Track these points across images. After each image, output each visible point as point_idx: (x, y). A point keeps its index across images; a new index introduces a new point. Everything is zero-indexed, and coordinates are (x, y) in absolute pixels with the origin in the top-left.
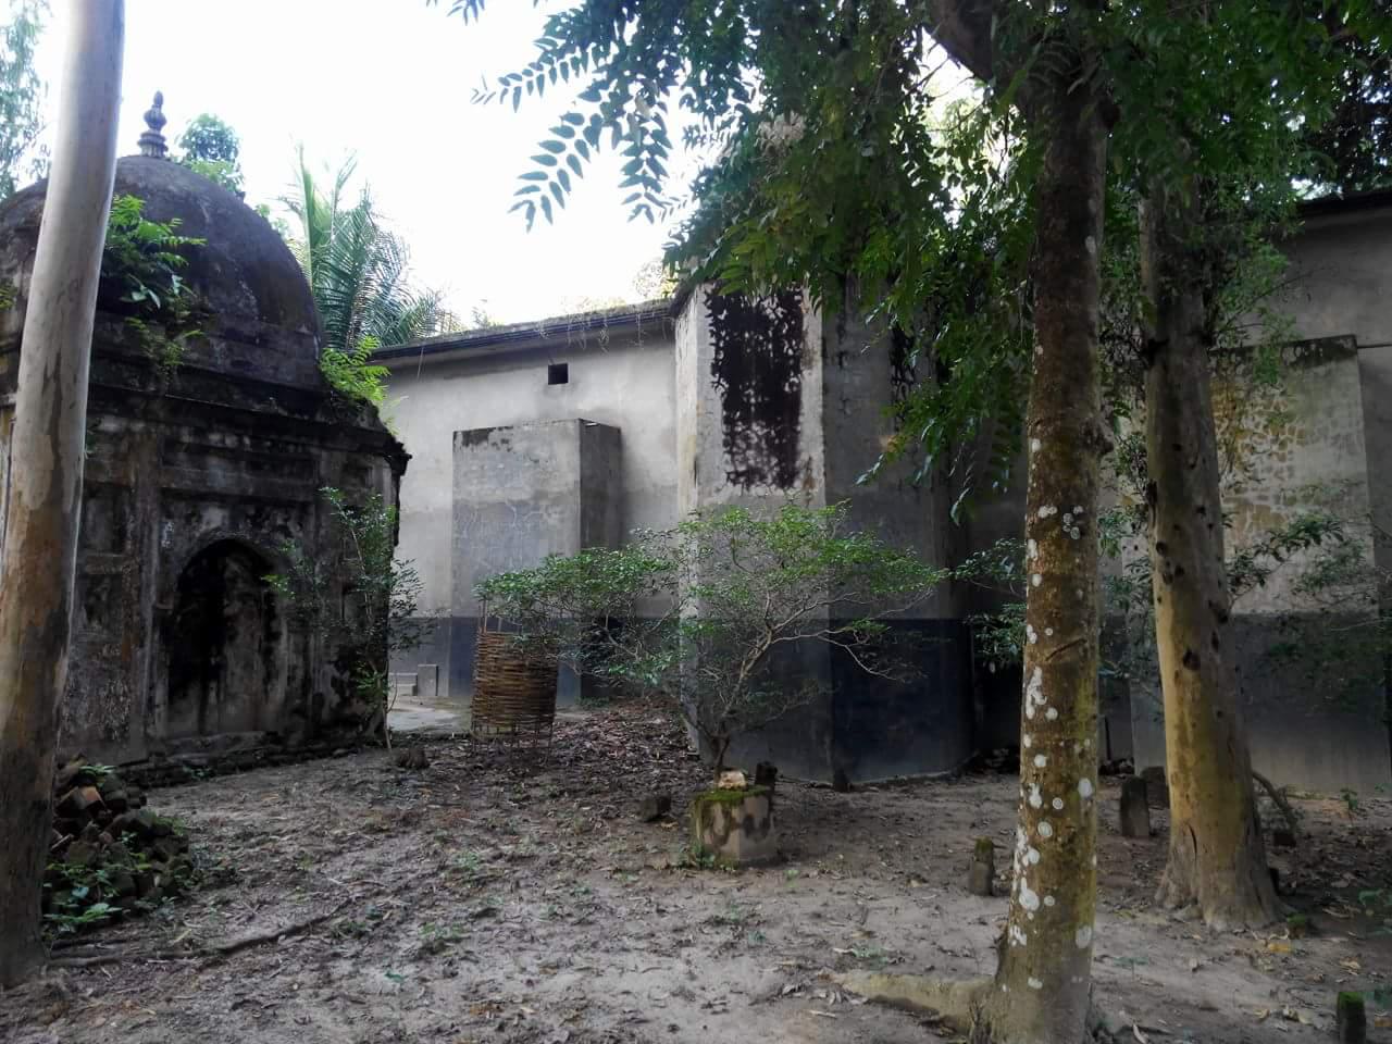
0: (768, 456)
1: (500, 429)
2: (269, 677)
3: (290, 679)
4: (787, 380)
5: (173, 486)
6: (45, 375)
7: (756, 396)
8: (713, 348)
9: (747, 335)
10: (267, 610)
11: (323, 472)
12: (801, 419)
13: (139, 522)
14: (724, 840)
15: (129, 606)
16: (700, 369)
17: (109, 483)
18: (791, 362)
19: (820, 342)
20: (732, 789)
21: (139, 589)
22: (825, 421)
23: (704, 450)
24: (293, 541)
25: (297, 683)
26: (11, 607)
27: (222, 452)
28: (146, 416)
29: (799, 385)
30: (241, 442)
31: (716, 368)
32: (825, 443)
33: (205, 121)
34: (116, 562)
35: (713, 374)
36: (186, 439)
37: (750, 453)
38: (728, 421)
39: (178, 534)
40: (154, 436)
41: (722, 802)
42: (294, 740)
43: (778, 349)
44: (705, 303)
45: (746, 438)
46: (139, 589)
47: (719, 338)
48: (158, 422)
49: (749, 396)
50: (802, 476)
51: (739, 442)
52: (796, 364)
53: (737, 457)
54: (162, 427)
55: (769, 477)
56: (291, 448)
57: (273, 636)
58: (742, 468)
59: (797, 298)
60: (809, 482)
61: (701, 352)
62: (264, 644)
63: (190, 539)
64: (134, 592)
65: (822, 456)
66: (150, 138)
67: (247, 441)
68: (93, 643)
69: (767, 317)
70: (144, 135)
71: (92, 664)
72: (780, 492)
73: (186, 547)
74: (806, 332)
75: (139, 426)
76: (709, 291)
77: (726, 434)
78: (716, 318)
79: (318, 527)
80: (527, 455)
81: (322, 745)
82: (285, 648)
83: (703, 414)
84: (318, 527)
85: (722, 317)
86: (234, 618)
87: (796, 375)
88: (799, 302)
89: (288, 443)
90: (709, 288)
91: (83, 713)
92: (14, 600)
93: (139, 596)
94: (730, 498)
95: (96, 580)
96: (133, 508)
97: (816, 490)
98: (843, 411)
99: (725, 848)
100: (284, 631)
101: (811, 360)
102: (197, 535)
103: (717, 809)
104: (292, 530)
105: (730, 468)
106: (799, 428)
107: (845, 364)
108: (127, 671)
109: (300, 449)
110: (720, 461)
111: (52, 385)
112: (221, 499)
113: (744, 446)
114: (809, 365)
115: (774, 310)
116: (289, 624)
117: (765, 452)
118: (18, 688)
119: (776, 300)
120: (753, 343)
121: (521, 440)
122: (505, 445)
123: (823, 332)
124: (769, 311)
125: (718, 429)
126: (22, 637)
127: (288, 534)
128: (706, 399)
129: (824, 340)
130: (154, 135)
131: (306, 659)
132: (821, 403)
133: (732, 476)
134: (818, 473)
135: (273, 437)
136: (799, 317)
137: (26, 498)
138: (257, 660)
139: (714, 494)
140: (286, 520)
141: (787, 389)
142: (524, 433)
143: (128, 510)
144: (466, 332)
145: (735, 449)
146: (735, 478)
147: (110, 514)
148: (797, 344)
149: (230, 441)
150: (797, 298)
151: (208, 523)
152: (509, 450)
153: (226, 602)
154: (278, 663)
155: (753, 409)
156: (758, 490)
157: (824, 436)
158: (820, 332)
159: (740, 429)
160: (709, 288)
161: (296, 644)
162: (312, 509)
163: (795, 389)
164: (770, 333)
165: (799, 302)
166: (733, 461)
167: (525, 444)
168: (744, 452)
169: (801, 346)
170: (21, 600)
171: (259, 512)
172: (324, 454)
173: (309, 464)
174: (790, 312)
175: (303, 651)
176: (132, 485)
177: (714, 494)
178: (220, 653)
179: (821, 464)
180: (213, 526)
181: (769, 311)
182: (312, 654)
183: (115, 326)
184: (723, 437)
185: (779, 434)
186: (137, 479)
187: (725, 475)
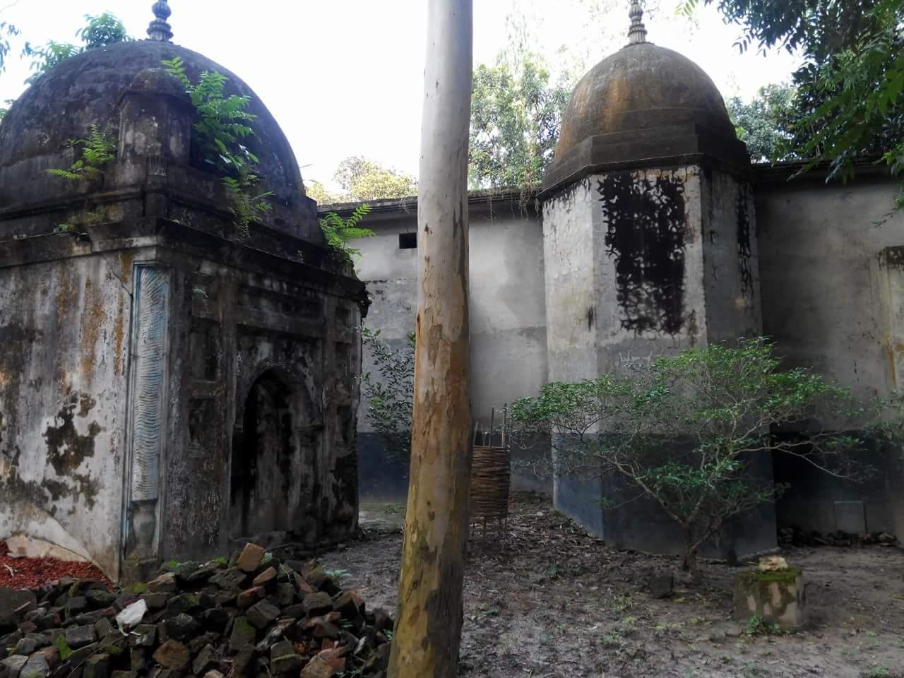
0: (657, 308)
1: (375, 282)
2: (286, 487)
3: (303, 486)
4: (672, 251)
5: (245, 323)
6: (454, 220)
7: (645, 262)
8: (607, 224)
9: (636, 216)
10: (286, 432)
11: (325, 313)
12: (685, 281)
13: (225, 353)
14: (782, 611)
15: (219, 426)
16: (595, 241)
17: (206, 319)
18: (675, 237)
19: (700, 223)
20: (778, 570)
21: (225, 411)
22: (705, 282)
23: (600, 302)
24: (308, 370)
25: (309, 490)
26: (442, 430)
27: (270, 295)
28: (230, 264)
29: (682, 255)
30: (282, 287)
31: (609, 240)
32: (706, 299)
33: (106, 20)
34: (212, 387)
35: (607, 244)
36: (252, 283)
37: (642, 306)
38: (620, 280)
39: (245, 364)
40: (233, 279)
41: (779, 582)
42: (311, 536)
43: (664, 226)
44: (599, 190)
45: (638, 295)
46: (225, 411)
47: (611, 217)
48: (235, 267)
49: (639, 262)
50: (687, 324)
51: (631, 297)
52: (680, 238)
53: (629, 309)
54: (238, 272)
55: (659, 324)
56: (309, 293)
57: (289, 450)
58: (634, 317)
59: (678, 189)
60: (693, 329)
61: (596, 227)
62: (282, 457)
63: (251, 368)
64: (223, 414)
65: (704, 309)
66: (158, 26)
67: (285, 286)
68: (197, 459)
69: (654, 202)
70: (152, 24)
71: (197, 477)
72: (668, 336)
73: (249, 375)
74: (688, 216)
75: (224, 271)
76: (602, 181)
77: (619, 291)
78: (608, 202)
79: (324, 358)
80: (400, 303)
81: (326, 541)
82: (298, 457)
83: (599, 275)
84: (324, 358)
85: (614, 201)
86: (261, 435)
87: (679, 248)
88: (681, 192)
89: (307, 289)
90: (602, 178)
91: (191, 521)
92: (444, 424)
93: (225, 417)
94: (625, 340)
95: (196, 403)
96: (221, 341)
97: (699, 335)
98: (714, 275)
99: (783, 617)
100: (298, 446)
101: (693, 236)
102: (255, 364)
103: (774, 588)
104: (307, 361)
105: (624, 317)
106: (683, 288)
107: (714, 240)
108: (218, 484)
109: (313, 294)
110: (613, 310)
111: (459, 230)
112: (269, 334)
113: (636, 300)
114: (691, 240)
115: (659, 198)
116: (301, 440)
117: (654, 306)
118: (452, 507)
119: (661, 190)
120: (641, 221)
121: (395, 291)
122: (380, 296)
123: (702, 215)
124: (654, 198)
125: (613, 287)
126: (453, 458)
127: (305, 365)
128: (601, 263)
129: (702, 221)
130: (160, 23)
131: (315, 469)
132: (702, 269)
133: (626, 323)
134: (701, 322)
135: (300, 283)
136: (681, 204)
137: (447, 331)
138: (276, 469)
139: (609, 337)
140: (304, 353)
141: (672, 258)
142: (397, 285)
143: (217, 342)
144: (334, 205)
145: (628, 303)
146: (628, 325)
147: (204, 346)
148: (680, 224)
149: (276, 286)
150: (678, 189)
151: (261, 355)
152: (383, 299)
153: (258, 421)
154: (294, 473)
155: (643, 272)
156: (648, 334)
157: (705, 294)
158: (699, 215)
159: (632, 287)
160: (602, 178)
161: (307, 457)
162: (319, 344)
163: (679, 258)
164: (656, 215)
165: (681, 192)
166: (626, 311)
167: (399, 295)
168: (636, 305)
169: (683, 225)
170: (451, 424)
171: (289, 344)
172: (326, 299)
173: (316, 306)
174: (673, 198)
175: (312, 462)
176: (220, 321)
177: (609, 337)
178: (256, 466)
179: (703, 315)
180: (264, 357)
181: (654, 198)
182: (320, 464)
183: (208, 184)
184: (617, 293)
185: (666, 292)
186: (223, 317)
187: (619, 323)
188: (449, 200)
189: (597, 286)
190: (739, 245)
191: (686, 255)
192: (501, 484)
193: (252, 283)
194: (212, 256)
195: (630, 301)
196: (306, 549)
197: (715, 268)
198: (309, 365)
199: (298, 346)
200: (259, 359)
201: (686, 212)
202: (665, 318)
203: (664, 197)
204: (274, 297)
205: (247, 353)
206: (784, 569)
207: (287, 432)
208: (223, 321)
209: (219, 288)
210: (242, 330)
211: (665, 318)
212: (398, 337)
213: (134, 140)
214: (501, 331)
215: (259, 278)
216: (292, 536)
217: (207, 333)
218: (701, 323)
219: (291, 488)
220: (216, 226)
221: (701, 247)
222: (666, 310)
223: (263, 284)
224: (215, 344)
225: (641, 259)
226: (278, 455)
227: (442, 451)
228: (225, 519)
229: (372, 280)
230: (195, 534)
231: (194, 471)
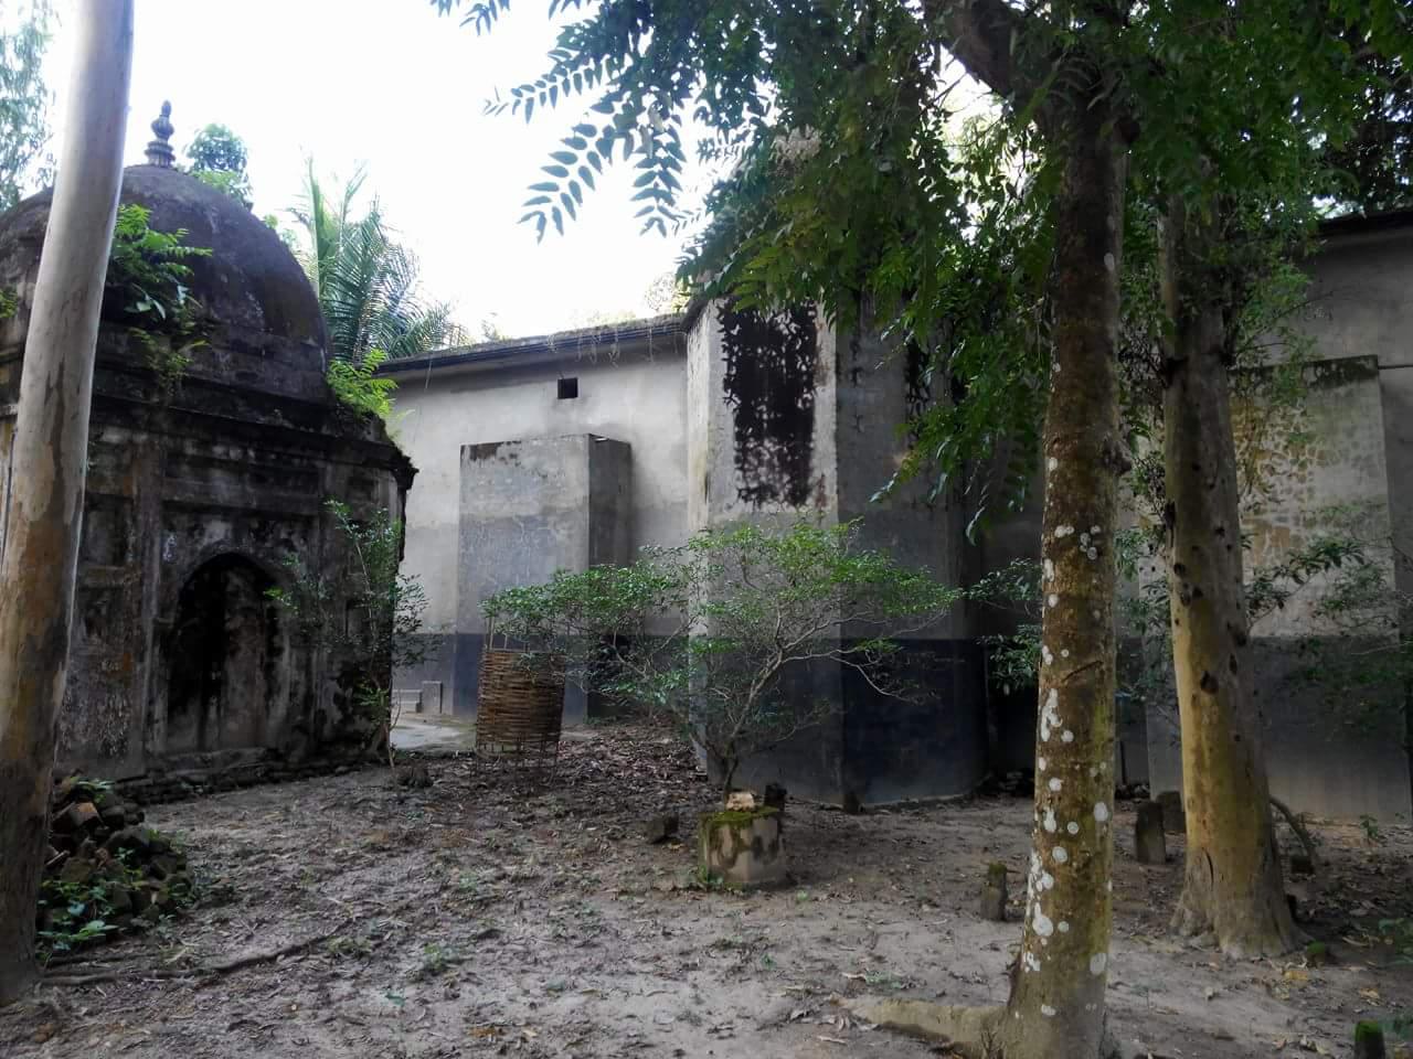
0: (781, 473)
1: (509, 443)
2: (270, 693)
3: (292, 695)
5: (176, 498)
8: (725, 363)
9: (760, 351)
12: (814, 436)
13: (141, 535)
14: (732, 862)
16: (711, 384)
18: (805, 378)
19: (834, 358)
20: (741, 810)
24: (296, 555)
27: (224, 464)
28: (150, 427)
29: (812, 401)
31: (728, 384)
32: (838, 460)
33: (213, 131)
34: (116, 575)
36: (190, 450)
37: (762, 470)
38: (740, 437)
40: (157, 447)
43: (791, 364)
44: (718, 318)
45: (759, 455)
46: (140, 603)
47: (732, 353)
48: (161, 433)
49: (761, 412)
50: (814, 493)
51: (751, 458)
52: (809, 381)
53: (748, 474)
54: (166, 438)
57: (275, 651)
58: (754, 485)
59: (810, 313)
60: (821, 500)
61: (713, 367)
62: (266, 660)
67: (251, 453)
69: (780, 332)
70: (151, 144)
72: (792, 509)
75: (142, 438)
76: (722, 306)
77: (738, 450)
79: (322, 540)
80: (536, 470)
81: (323, 762)
82: (286, 663)
83: (715, 430)
84: (322, 540)
85: (734, 332)
88: (813, 317)
89: (293, 456)
90: (722, 303)
94: (742, 515)
96: (134, 520)
97: (829, 508)
98: (857, 427)
99: (733, 871)
101: (825, 376)
102: (200, 548)
103: (725, 831)
104: (296, 543)
105: (742, 485)
106: (812, 445)
107: (859, 381)
110: (731, 477)
111: (55, 394)
112: (225, 512)
114: (823, 381)
115: (787, 326)
116: (291, 639)
118: (15, 702)
119: (790, 315)
121: (529, 455)
124: (782, 326)
125: (730, 445)
128: (718, 415)
129: (838, 356)
131: (308, 674)
132: (834, 420)
133: (744, 493)
134: (831, 490)
136: (813, 333)
137: (26, 509)
138: (259, 673)
140: (290, 534)
141: (800, 405)
142: (532, 447)
143: (129, 522)
146: (746, 495)
147: (111, 526)
148: (811, 360)
149: (235, 454)
150: (810, 313)
151: (211, 537)
153: (227, 616)
154: (280, 679)
156: (769, 507)
157: (837, 453)
160: (722, 303)
162: (317, 523)
163: (808, 405)
164: (784, 349)
165: (813, 317)
168: (756, 469)
171: (263, 525)
172: (330, 468)
173: (313, 478)
175: (306, 667)
179: (835, 480)
180: (216, 539)
181: (782, 326)
183: (120, 336)
184: (735, 453)
185: (792, 451)
186: (139, 490)
187: (736, 492)
188: (43, 363)
189: (712, 445)
190: (908, 387)
191: (817, 402)
192: (541, 698)
193: (190, 450)
194: (119, 421)
195: (750, 464)
196: (285, 769)
197: (858, 419)
198: (299, 548)
199: (279, 525)
200: (206, 541)
201: (818, 344)
202: (789, 486)
203: (793, 325)
204: (236, 469)
205: (186, 534)
206: (748, 808)
207: (272, 629)
208: (138, 497)
209: (133, 457)
210: (170, 509)
211: (789, 486)
212: (532, 512)
213: (25, 293)
214: (673, 504)
215: (205, 444)
216: (274, 754)
217: (117, 512)
218: (831, 491)
219: (275, 697)
220: (130, 385)
221: (834, 390)
222: (791, 474)
223: (212, 452)
224: (126, 525)
225: (764, 408)
226: (262, 658)
227: (7, 643)
228: (137, 727)
229: (506, 440)
230: (88, 743)
231: (87, 671)
